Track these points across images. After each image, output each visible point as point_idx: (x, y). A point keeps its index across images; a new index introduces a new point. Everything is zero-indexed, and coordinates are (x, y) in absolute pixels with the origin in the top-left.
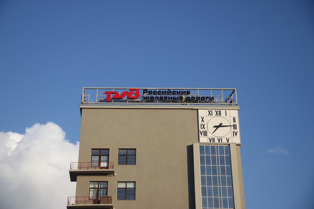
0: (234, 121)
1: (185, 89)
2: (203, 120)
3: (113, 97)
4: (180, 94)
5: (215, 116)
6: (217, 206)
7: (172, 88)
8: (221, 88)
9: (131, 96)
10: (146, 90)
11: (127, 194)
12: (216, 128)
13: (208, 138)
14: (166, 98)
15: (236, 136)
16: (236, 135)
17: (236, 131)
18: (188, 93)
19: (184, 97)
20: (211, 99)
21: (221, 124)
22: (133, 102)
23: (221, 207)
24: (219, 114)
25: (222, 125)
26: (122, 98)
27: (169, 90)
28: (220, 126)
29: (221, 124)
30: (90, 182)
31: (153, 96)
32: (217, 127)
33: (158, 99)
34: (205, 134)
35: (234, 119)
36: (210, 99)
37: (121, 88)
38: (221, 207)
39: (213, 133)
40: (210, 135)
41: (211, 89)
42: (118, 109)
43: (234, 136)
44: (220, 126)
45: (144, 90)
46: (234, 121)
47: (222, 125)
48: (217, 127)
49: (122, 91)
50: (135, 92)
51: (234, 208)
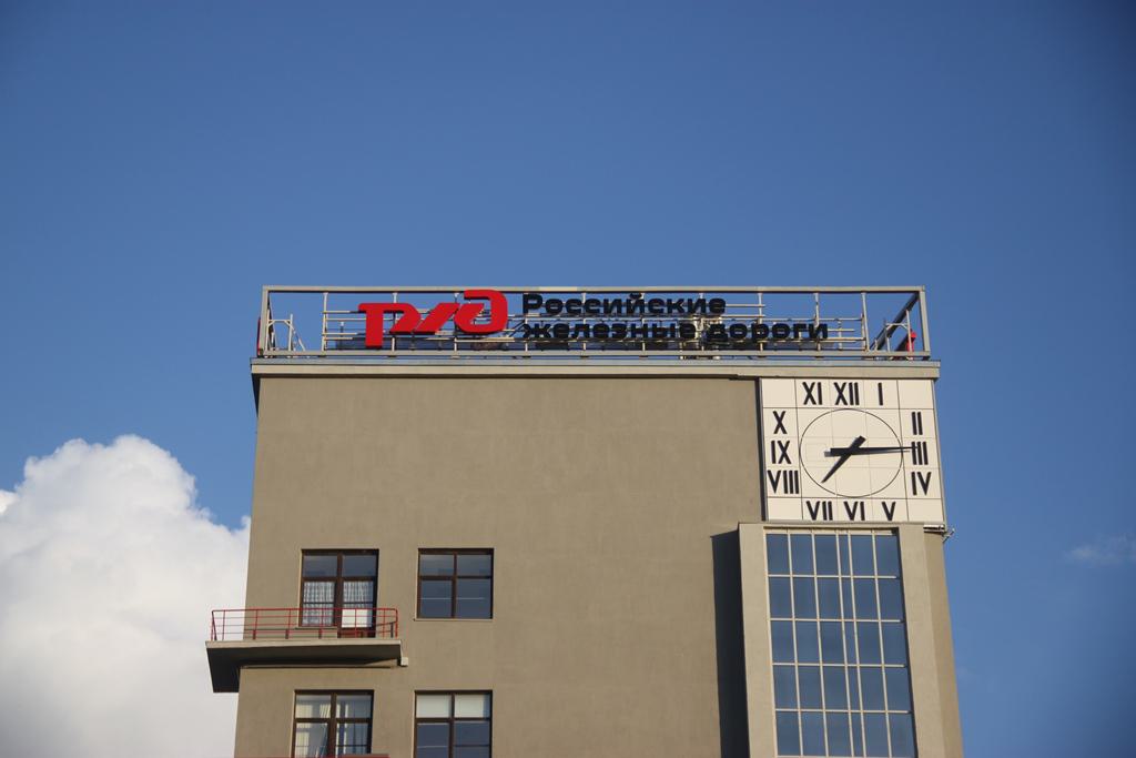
2: (780, 425)
3: (393, 328)
4: (681, 310)
7: (646, 289)
9: (470, 323)
10: (536, 296)
14: (620, 329)
15: (926, 492)
16: (925, 487)
18: (718, 306)
19: (699, 325)
20: (817, 334)
21: (861, 440)
24: (849, 396)
25: (863, 446)
26: (432, 333)
28: (857, 448)
29: (861, 440)
30: (298, 692)
31: (564, 320)
32: (842, 454)
34: (792, 483)
37: (425, 285)
39: (825, 480)
40: (809, 489)
43: (915, 493)
44: (857, 448)
45: (528, 297)
47: (863, 446)
48: (842, 454)
50: (487, 305)
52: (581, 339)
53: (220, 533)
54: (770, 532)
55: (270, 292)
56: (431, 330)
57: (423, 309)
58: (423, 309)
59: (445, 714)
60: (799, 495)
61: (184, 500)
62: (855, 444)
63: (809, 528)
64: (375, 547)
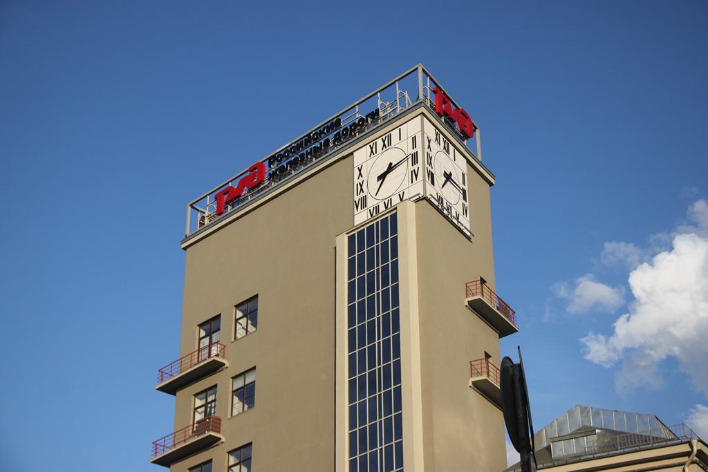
0: (414, 146)
1: (231, 181)
2: (360, 174)
3: (228, 198)
5: (364, 165)
6: (374, 467)
7: (311, 129)
9: (253, 181)
10: (273, 157)
11: (243, 453)
12: (208, 337)
14: (302, 156)
16: (416, 176)
17: (415, 167)
19: (331, 137)
22: (262, 189)
23: (381, 470)
24: (387, 143)
25: (393, 165)
26: (240, 196)
27: (308, 135)
28: (391, 168)
29: (391, 164)
32: (382, 177)
36: (373, 118)
37: (230, 176)
38: (381, 470)
40: (371, 203)
41: (356, 103)
44: (391, 168)
46: (414, 146)
47: (393, 165)
48: (382, 177)
52: (310, 158)
53: (581, 285)
54: (349, 235)
55: (423, 113)
56: (237, 194)
57: (235, 185)
58: (235, 185)
59: (242, 385)
61: (672, 256)
63: (362, 226)
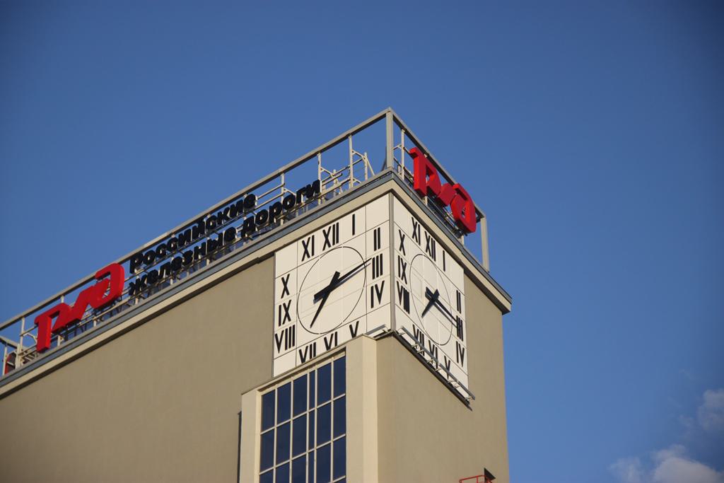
0: (377, 244)
1: (64, 294)
2: (286, 289)
7: (205, 210)
8: (313, 149)
9: (103, 295)
10: (138, 255)
13: (298, 350)
16: (379, 296)
19: (238, 225)
20: (312, 190)
21: (337, 274)
24: (333, 238)
27: (200, 221)
28: (337, 281)
29: (337, 274)
31: (188, 249)
32: (322, 296)
33: (203, 254)
34: (290, 335)
35: (377, 234)
37: (63, 282)
39: (311, 325)
41: (281, 170)
42: (68, 366)
43: (372, 306)
44: (337, 281)
45: (132, 258)
46: (377, 244)
47: (285, 293)
48: (322, 296)
49: (283, 198)
51: (238, 481)
57: (71, 301)
60: (295, 347)
62: (357, 281)
64: (494, 474)
